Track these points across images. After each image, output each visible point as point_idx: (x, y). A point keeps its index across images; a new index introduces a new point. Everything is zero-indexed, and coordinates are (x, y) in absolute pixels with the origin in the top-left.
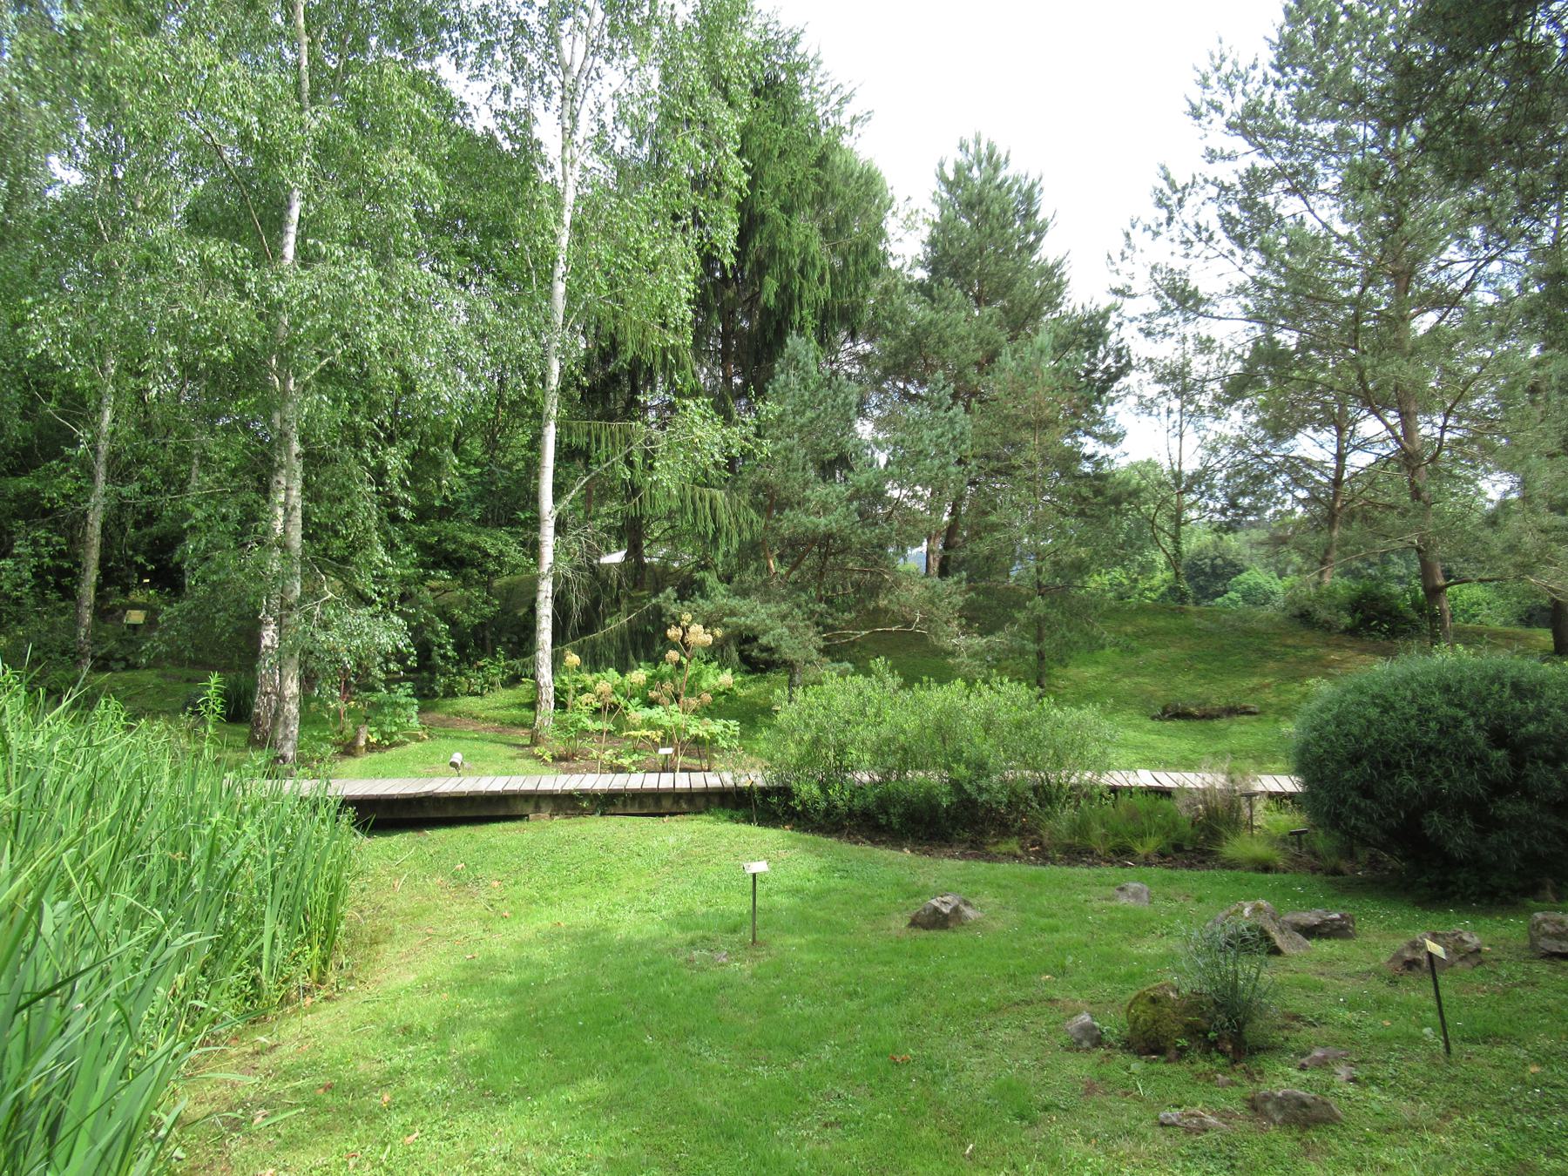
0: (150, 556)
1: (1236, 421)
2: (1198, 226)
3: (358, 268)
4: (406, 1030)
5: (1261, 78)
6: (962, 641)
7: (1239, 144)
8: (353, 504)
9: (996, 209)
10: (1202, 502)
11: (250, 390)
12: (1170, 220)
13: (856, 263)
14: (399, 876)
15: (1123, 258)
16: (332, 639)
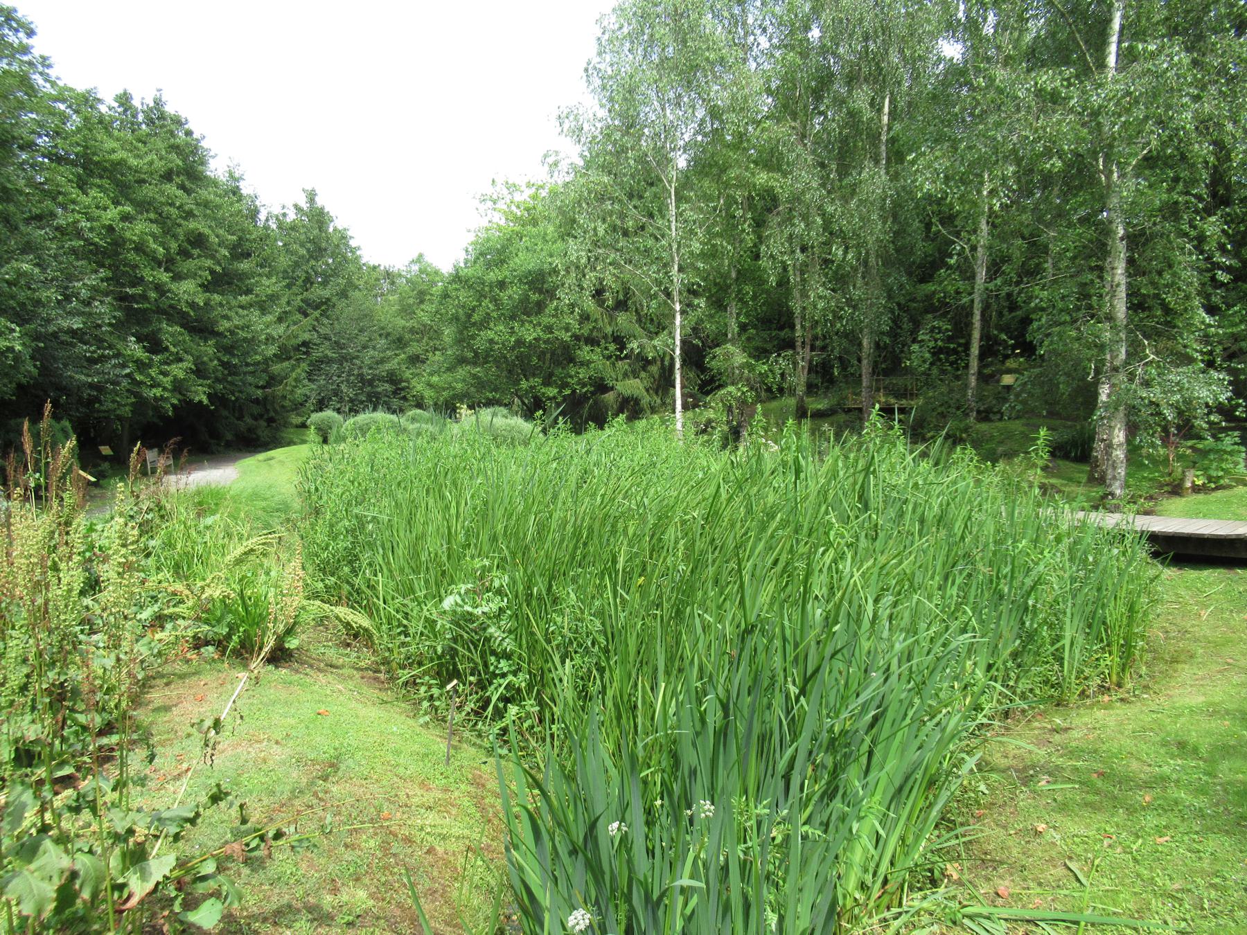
0: (1014, 334)
3: (1171, 56)
4: (1182, 745)
8: (1174, 275)
11: (1080, 187)
14: (1207, 607)
16: (1155, 394)
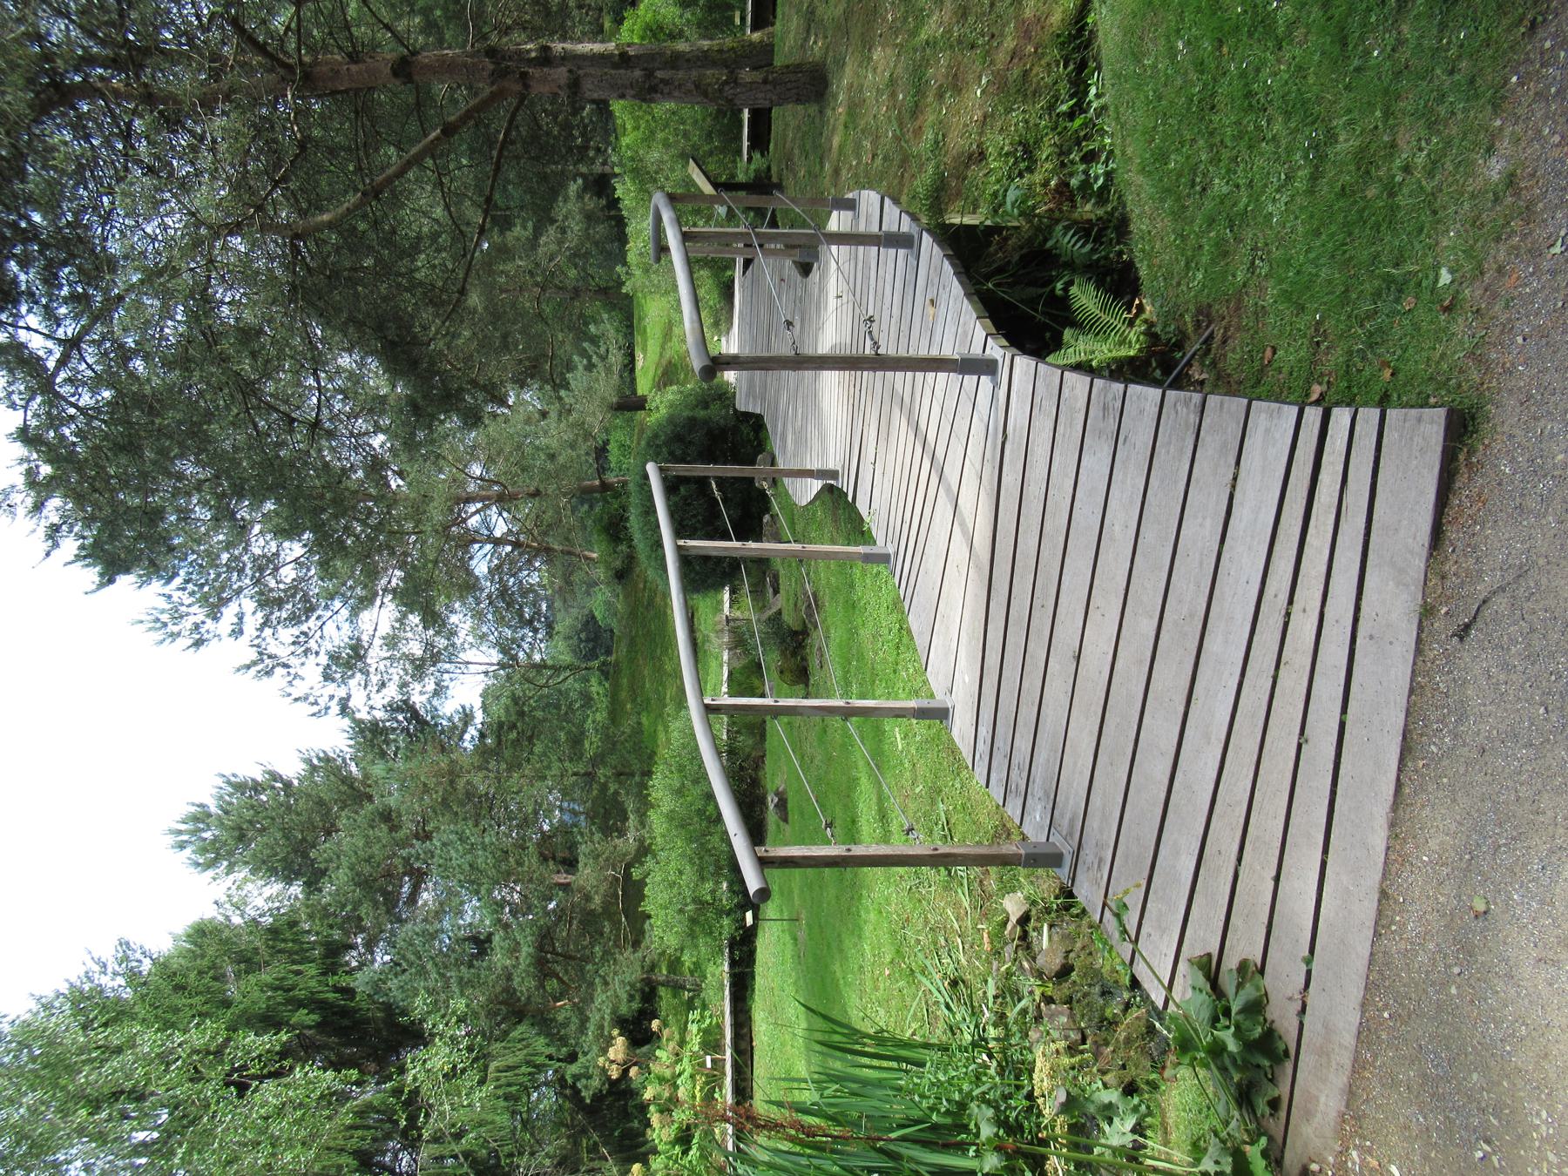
1: (460, 620)
2: (294, 643)
5: (180, 593)
6: (631, 836)
7: (229, 613)
9: (248, 814)
10: (526, 646)
12: (286, 666)
13: (284, 941)
15: (316, 703)
